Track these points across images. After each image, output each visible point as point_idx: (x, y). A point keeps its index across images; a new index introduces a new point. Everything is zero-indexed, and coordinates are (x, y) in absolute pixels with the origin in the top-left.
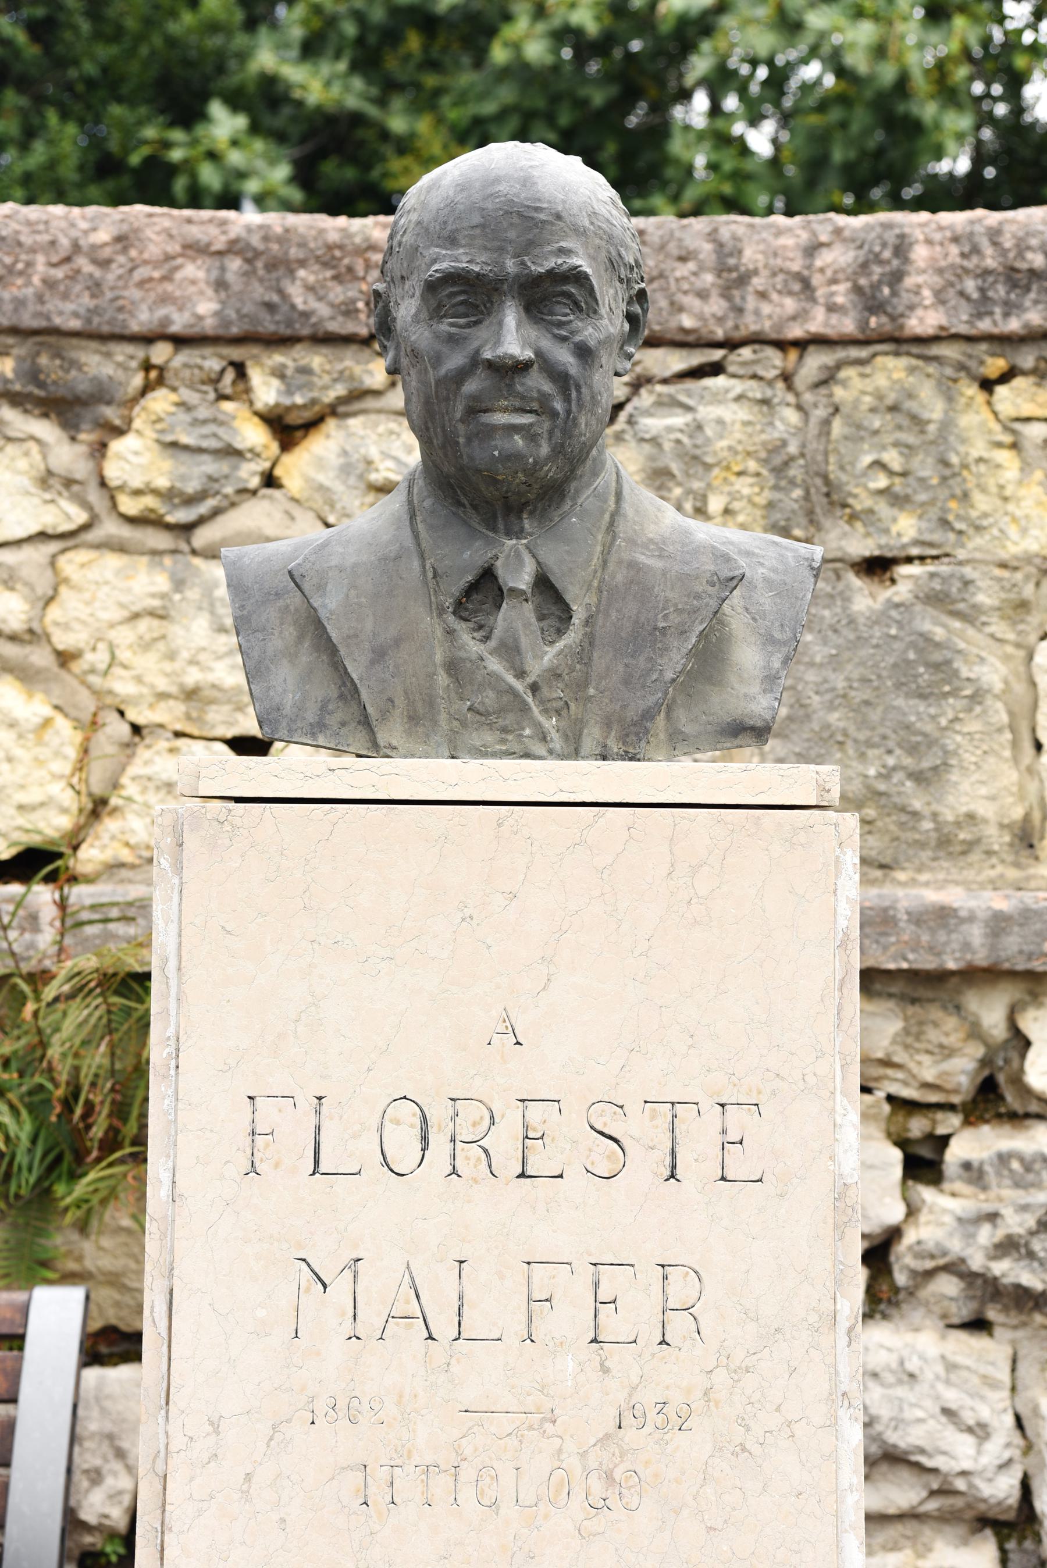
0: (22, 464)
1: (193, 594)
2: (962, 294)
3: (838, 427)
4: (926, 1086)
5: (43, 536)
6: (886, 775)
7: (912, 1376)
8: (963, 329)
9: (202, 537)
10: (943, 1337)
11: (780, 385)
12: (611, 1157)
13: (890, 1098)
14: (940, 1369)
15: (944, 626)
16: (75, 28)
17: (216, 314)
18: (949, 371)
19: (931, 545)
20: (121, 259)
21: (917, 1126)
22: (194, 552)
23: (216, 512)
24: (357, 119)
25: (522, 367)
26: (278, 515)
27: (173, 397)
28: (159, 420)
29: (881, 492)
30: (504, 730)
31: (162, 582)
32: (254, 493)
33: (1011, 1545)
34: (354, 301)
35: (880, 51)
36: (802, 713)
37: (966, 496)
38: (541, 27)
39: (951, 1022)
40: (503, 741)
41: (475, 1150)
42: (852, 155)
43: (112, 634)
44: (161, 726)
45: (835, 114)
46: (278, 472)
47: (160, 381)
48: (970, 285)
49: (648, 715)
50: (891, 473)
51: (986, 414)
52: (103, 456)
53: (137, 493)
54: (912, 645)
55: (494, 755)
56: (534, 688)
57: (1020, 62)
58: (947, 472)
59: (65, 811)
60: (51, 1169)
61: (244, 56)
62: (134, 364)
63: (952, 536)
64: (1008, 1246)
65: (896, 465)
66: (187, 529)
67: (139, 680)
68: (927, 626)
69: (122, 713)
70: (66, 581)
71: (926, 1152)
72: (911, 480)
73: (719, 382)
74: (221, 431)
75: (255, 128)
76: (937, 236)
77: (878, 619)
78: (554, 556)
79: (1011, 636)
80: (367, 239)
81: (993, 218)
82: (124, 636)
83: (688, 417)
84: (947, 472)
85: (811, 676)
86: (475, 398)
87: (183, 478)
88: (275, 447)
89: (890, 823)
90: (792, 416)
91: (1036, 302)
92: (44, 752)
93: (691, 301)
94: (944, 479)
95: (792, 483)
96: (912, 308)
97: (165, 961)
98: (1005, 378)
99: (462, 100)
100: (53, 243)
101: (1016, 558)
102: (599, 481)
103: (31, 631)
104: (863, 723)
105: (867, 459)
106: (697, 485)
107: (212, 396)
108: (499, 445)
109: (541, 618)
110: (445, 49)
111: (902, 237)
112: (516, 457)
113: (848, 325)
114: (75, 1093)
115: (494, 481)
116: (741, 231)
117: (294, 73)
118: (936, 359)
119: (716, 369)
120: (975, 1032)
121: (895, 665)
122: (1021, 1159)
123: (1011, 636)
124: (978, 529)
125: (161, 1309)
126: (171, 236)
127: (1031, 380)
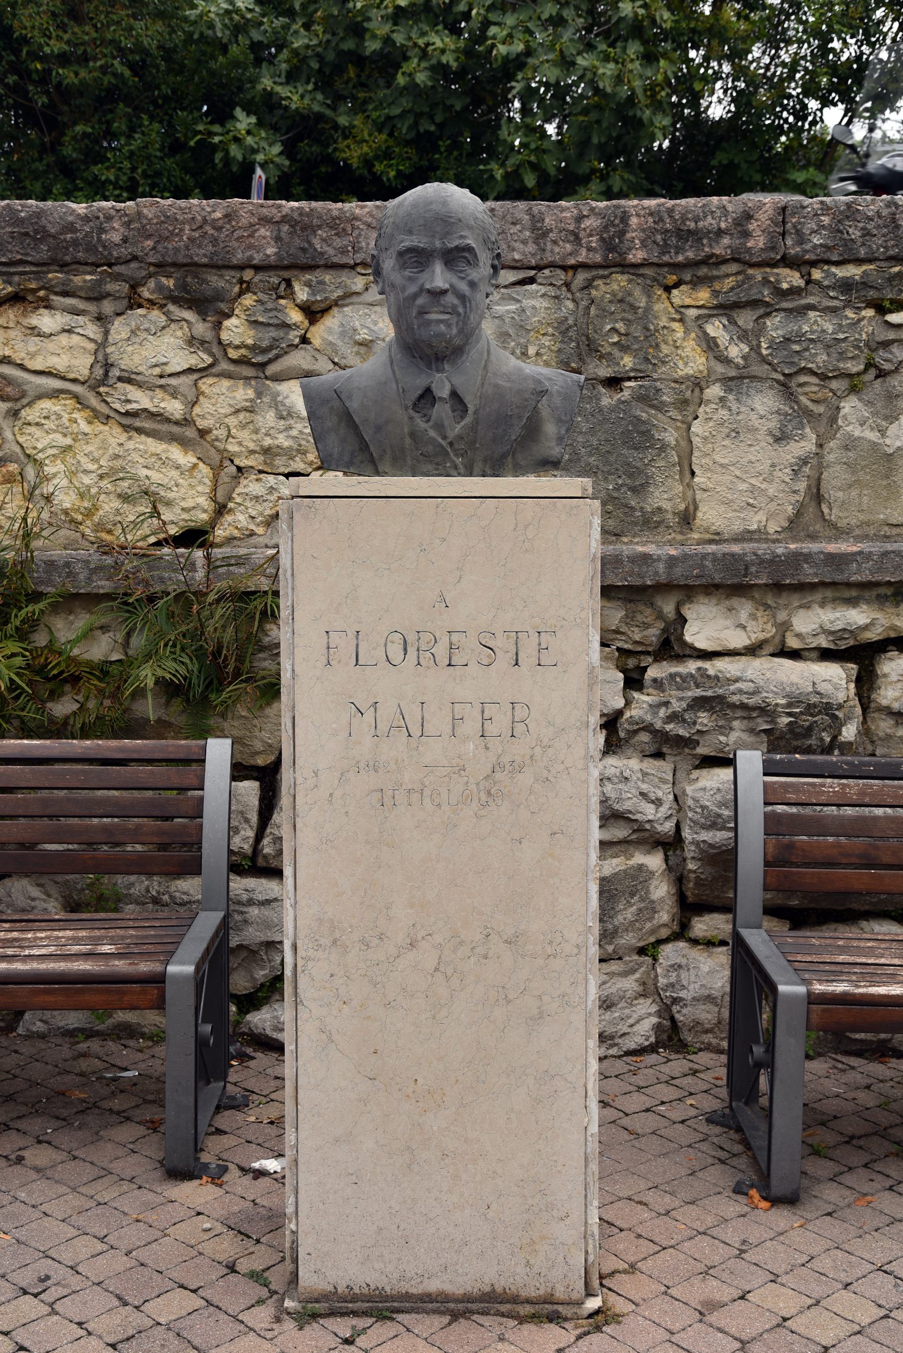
0: (179, 333)
1: (267, 399)
2: (654, 242)
3: (593, 311)
4: (636, 643)
5: (190, 370)
6: (617, 488)
7: (626, 778)
8: (655, 260)
9: (271, 369)
10: (642, 761)
11: (564, 289)
12: (489, 656)
13: (618, 649)
14: (640, 775)
15: (647, 412)
16: (157, 67)
17: (276, 254)
18: (648, 282)
19: (640, 371)
20: (228, 226)
21: (631, 663)
22: (266, 378)
23: (277, 357)
24: (320, 117)
25: (444, 292)
26: (309, 358)
27: (255, 297)
28: (248, 309)
29: (615, 344)
30: (437, 464)
31: (251, 393)
32: (297, 346)
33: (670, 853)
34: (347, 247)
35: (618, 79)
36: (576, 458)
37: (657, 345)
38: (424, 64)
39: (648, 611)
40: (437, 469)
41: (428, 654)
42: (603, 140)
43: (226, 420)
44: (252, 467)
45: (593, 116)
46: (308, 335)
47: (248, 290)
48: (659, 238)
49: (504, 456)
50: (620, 334)
51: (667, 304)
52: (220, 329)
53: (237, 347)
54: (631, 422)
55: (433, 476)
56: (451, 444)
57: (697, 86)
58: (648, 334)
59: (205, 511)
60: (207, 688)
61: (254, 81)
62: (234, 281)
63: (650, 366)
64: (673, 717)
65: (623, 331)
66: (263, 366)
67: (240, 444)
68: (638, 413)
69: (232, 461)
70: (203, 393)
71: (635, 676)
72: (630, 338)
73: (534, 286)
74: (279, 315)
75: (260, 124)
76: (642, 212)
77: (613, 409)
78: (459, 381)
79: (680, 418)
80: (353, 214)
81: (671, 203)
82: (232, 421)
83: (518, 305)
84: (648, 334)
85: (580, 439)
86: (422, 307)
87: (260, 339)
88: (306, 323)
89: (619, 513)
90: (570, 305)
91: (691, 247)
92: (194, 481)
93: (517, 245)
94: (646, 337)
95: (571, 339)
96: (630, 249)
97: (286, 571)
98: (677, 285)
99: (380, 106)
100: (193, 218)
101: (682, 377)
102: (479, 345)
103: (185, 419)
104: (607, 463)
105: (609, 327)
106: (522, 341)
107: (274, 296)
108: (434, 328)
109: (453, 411)
110: (369, 76)
111: (625, 212)
112: (442, 335)
113: (598, 258)
114: (220, 647)
115: (430, 346)
116: (543, 209)
117: (283, 91)
118: (642, 275)
119: (531, 281)
120: (660, 616)
121: (622, 432)
122: (681, 677)
123: (680, 418)
124: (664, 363)
125: (289, 725)
126: (253, 214)
127: (689, 286)
